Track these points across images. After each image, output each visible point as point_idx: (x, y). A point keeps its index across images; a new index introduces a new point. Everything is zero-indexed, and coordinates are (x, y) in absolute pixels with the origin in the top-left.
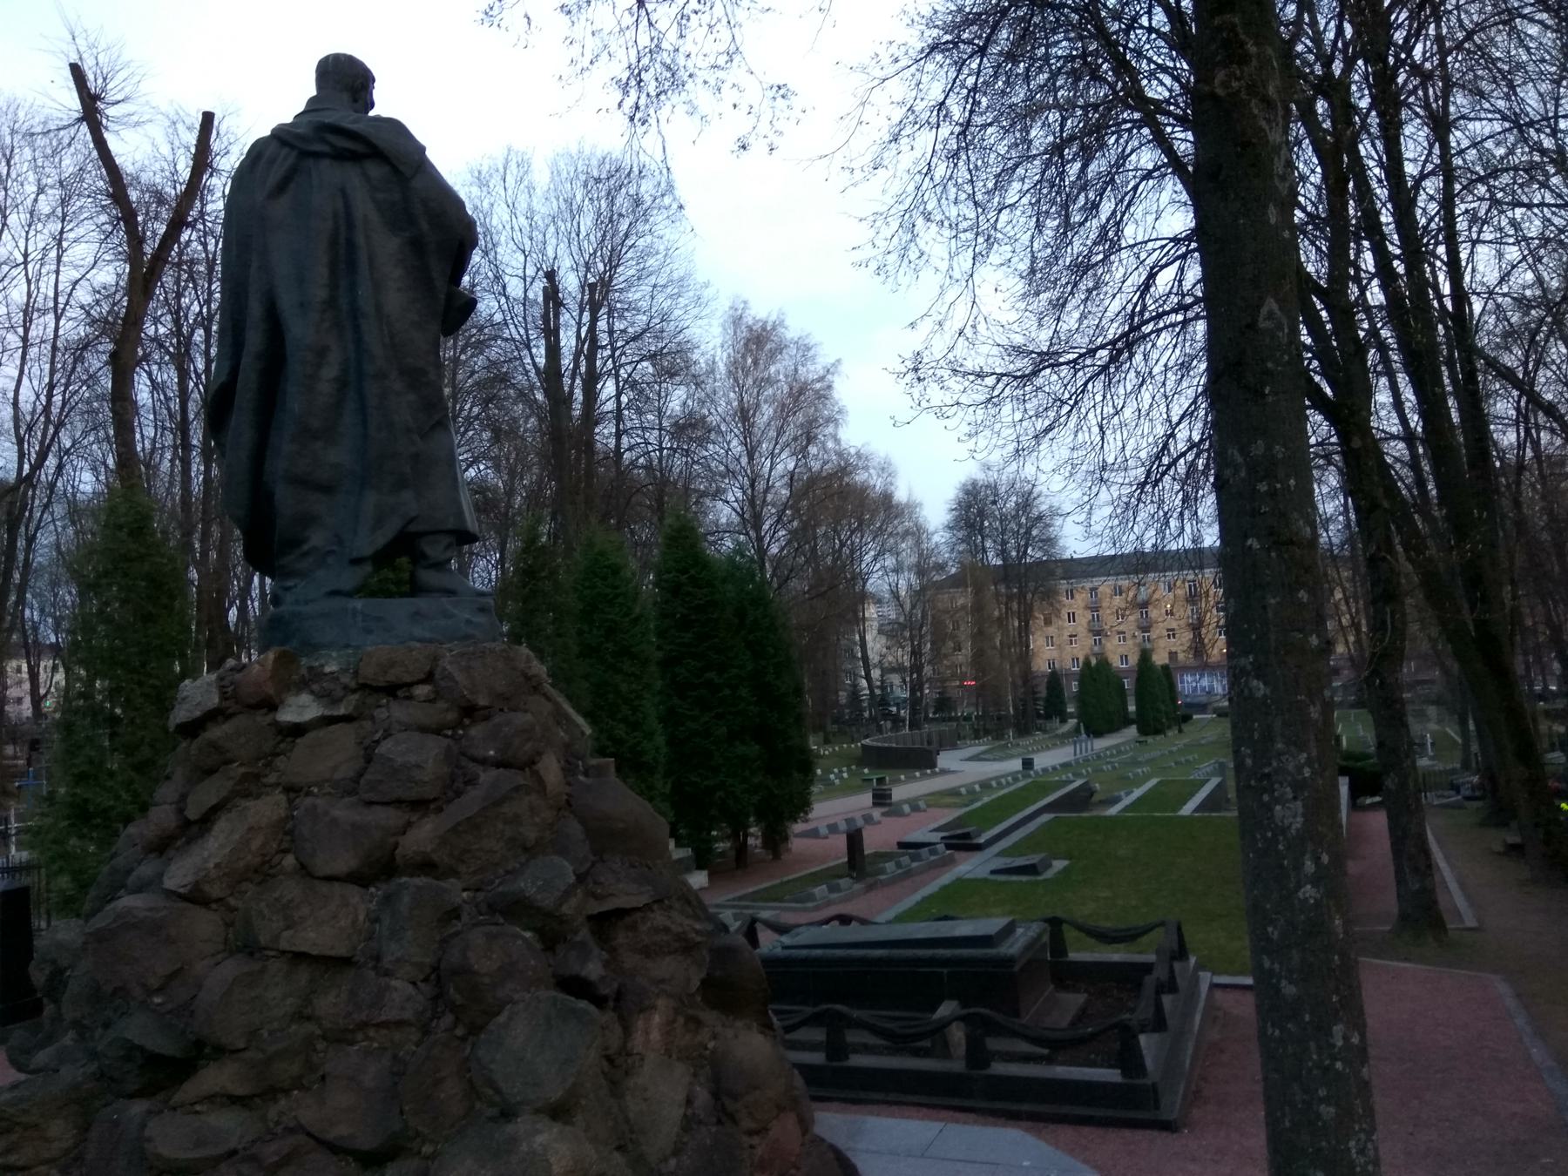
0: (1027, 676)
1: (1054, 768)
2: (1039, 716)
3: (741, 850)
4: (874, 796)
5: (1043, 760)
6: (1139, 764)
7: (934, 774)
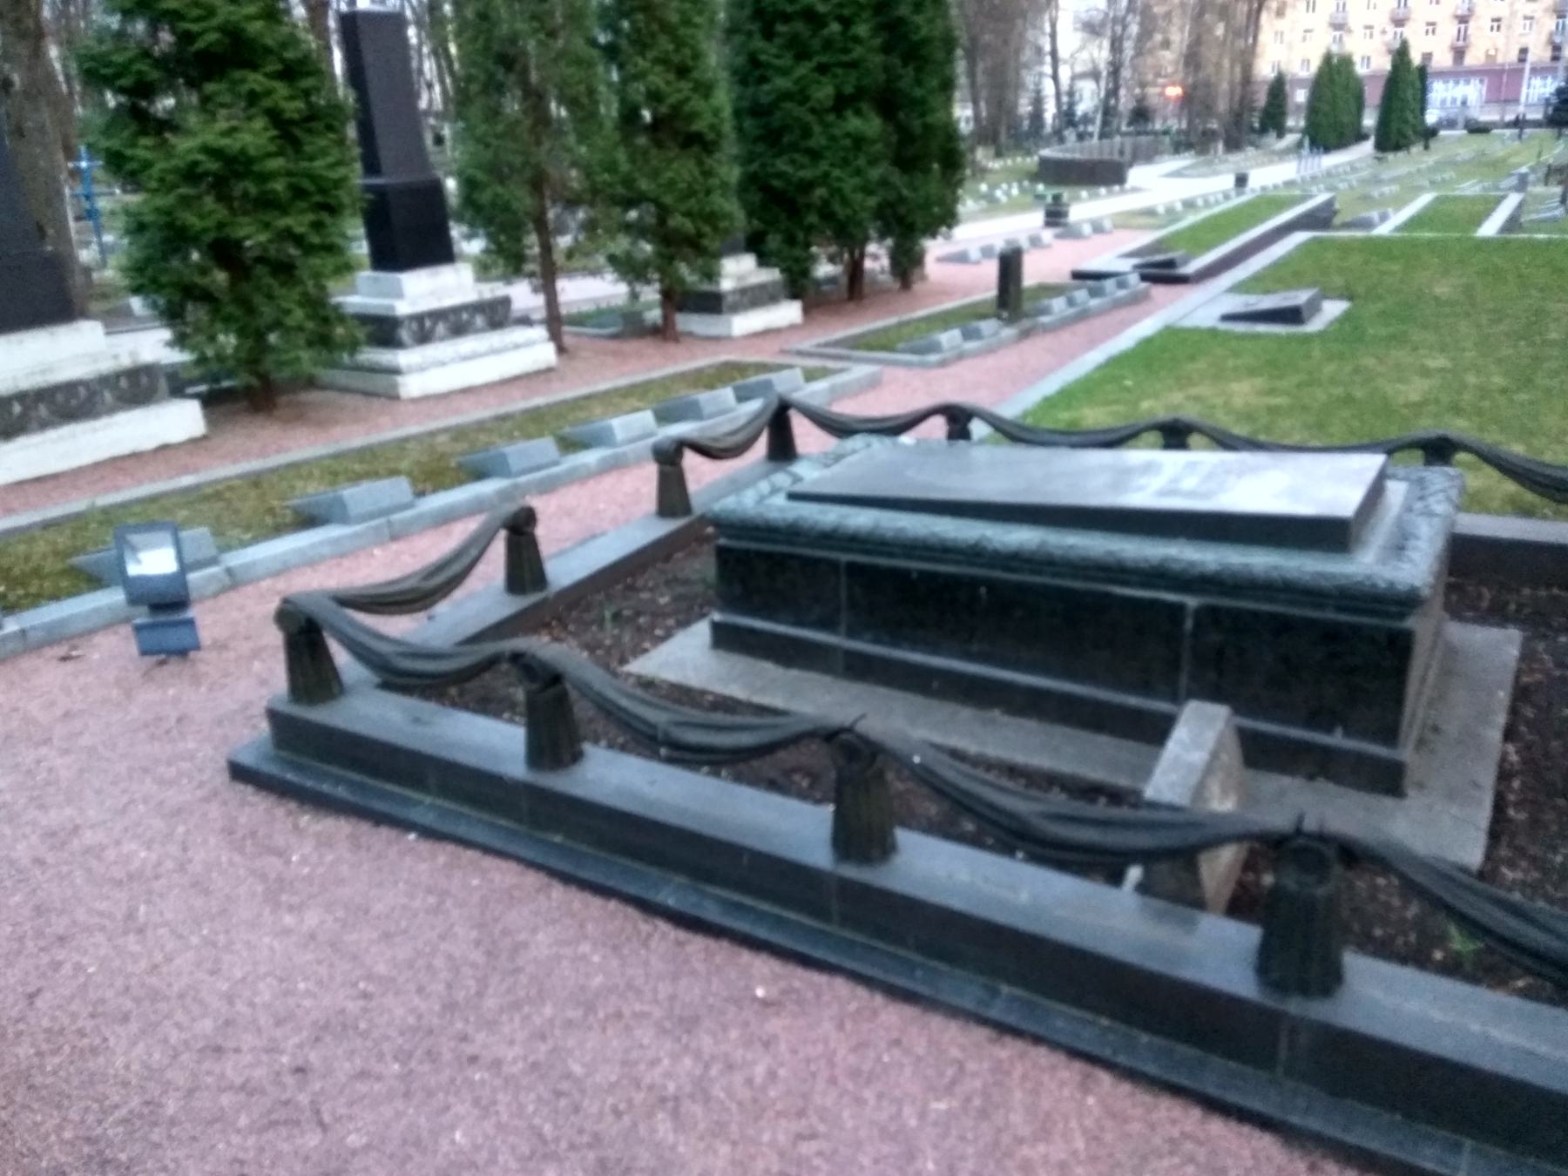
0: (1247, 79)
1: (1276, 187)
2: (1253, 130)
3: (855, 272)
7: (1123, 192)
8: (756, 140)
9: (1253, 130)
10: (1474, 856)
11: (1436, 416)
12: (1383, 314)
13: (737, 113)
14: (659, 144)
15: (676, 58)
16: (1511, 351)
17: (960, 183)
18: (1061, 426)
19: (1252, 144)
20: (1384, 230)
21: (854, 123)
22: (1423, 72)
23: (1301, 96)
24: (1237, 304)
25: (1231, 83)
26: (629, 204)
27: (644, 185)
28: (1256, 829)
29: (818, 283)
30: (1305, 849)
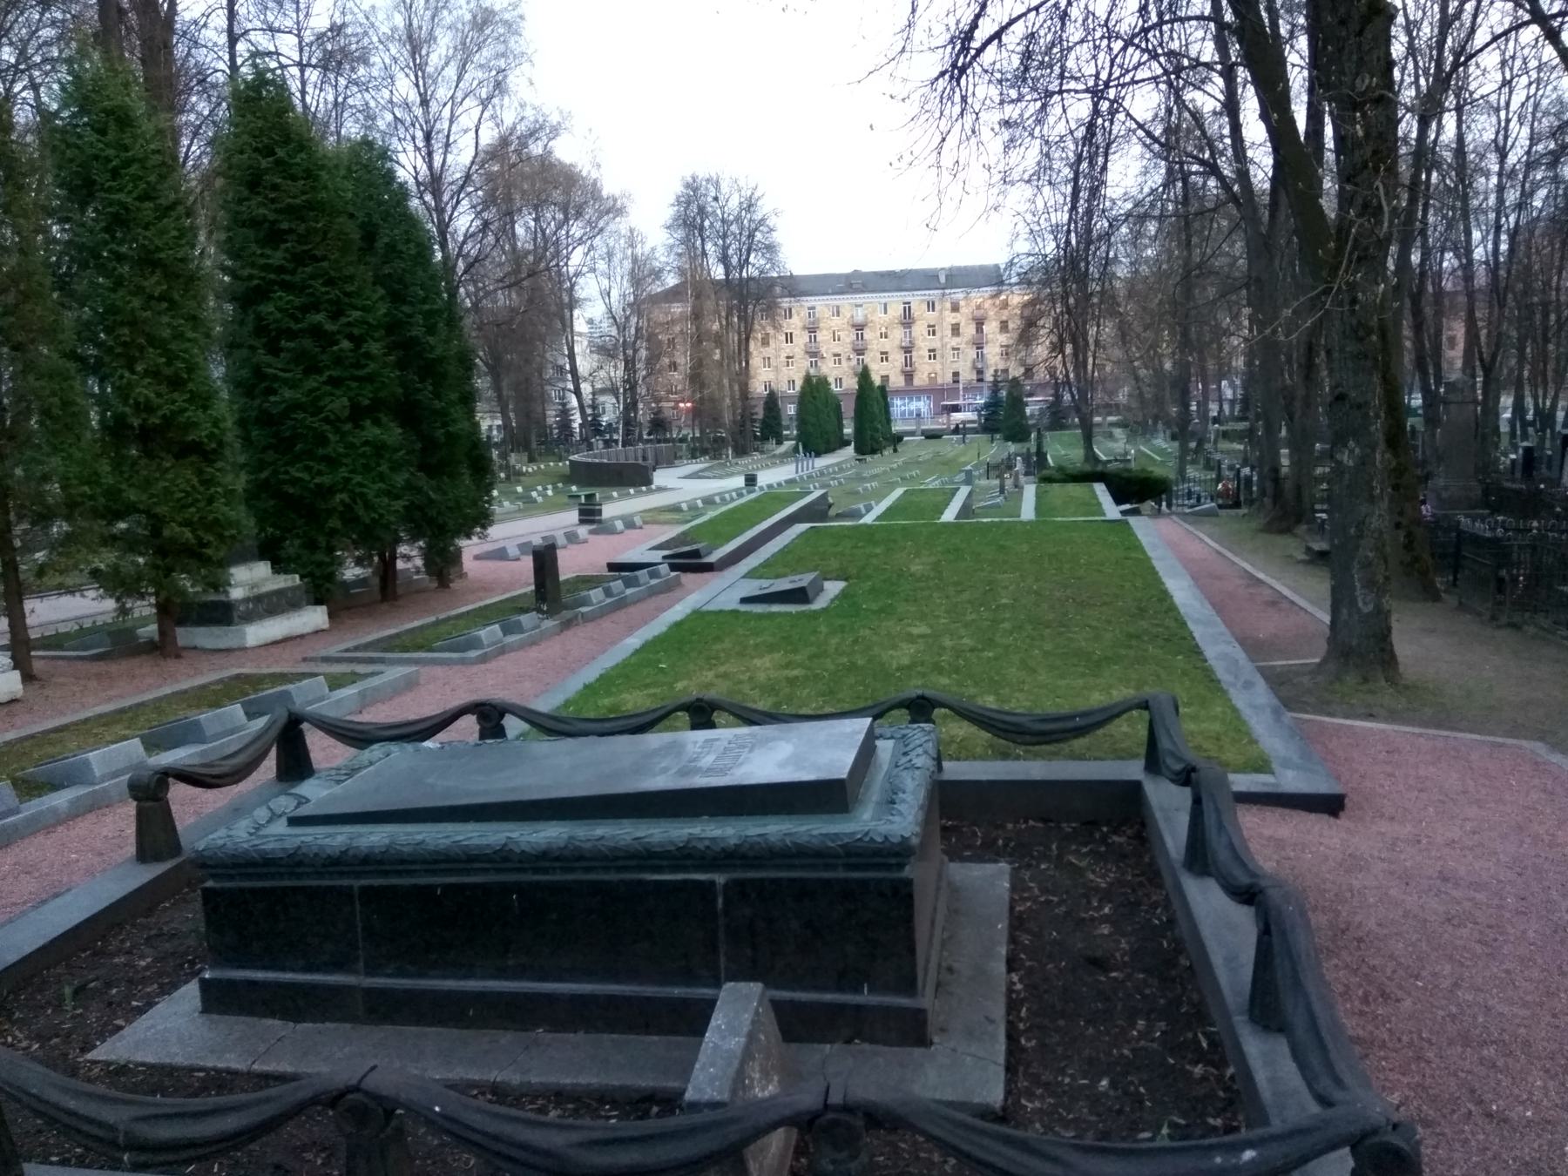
1: (779, 485)
3: (387, 572)
4: (582, 512)
5: (769, 477)
6: (863, 479)
7: (650, 491)
8: (265, 449)
9: (756, 437)
10: (994, 1094)
11: (924, 675)
12: (873, 590)
13: (242, 423)
14: (148, 454)
15: (168, 371)
16: (974, 616)
17: (490, 486)
18: (602, 713)
19: (756, 450)
20: (868, 519)
21: (371, 432)
22: (883, 388)
23: (791, 410)
24: (754, 587)
25: (732, 398)
26: (119, 516)
27: (132, 495)
28: (787, 1112)
29: (346, 585)
30: (835, 1123)
